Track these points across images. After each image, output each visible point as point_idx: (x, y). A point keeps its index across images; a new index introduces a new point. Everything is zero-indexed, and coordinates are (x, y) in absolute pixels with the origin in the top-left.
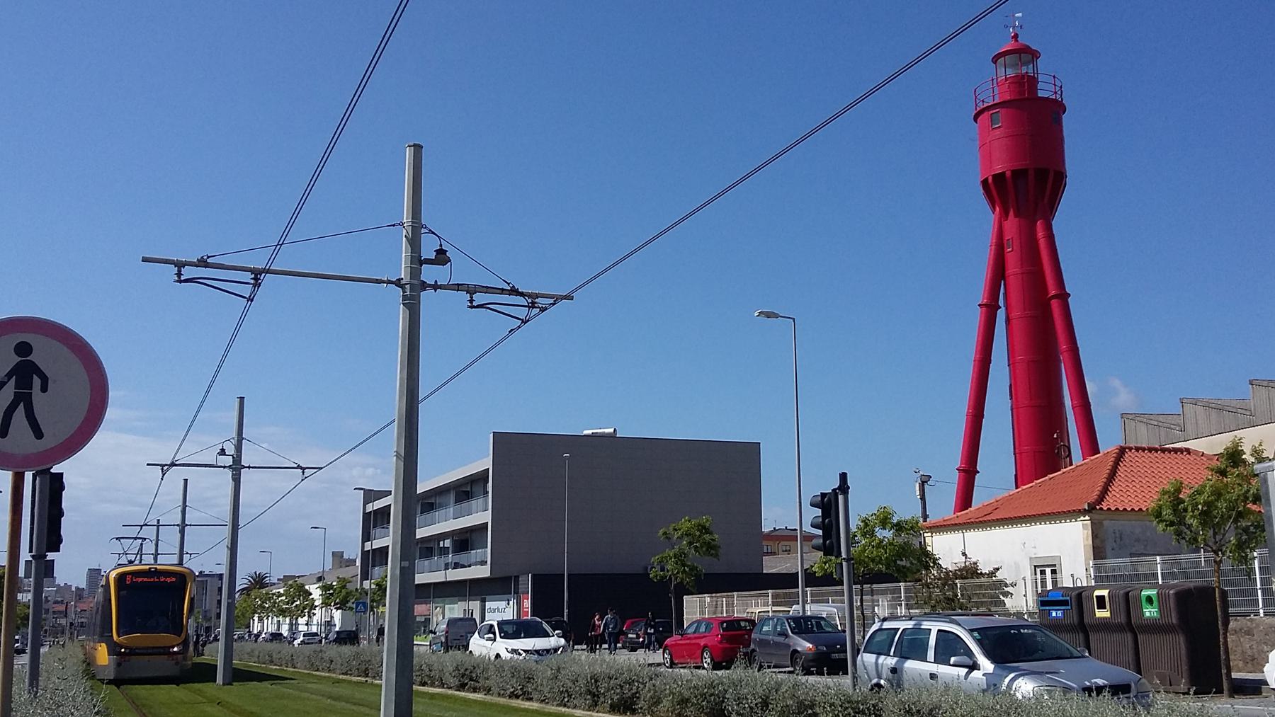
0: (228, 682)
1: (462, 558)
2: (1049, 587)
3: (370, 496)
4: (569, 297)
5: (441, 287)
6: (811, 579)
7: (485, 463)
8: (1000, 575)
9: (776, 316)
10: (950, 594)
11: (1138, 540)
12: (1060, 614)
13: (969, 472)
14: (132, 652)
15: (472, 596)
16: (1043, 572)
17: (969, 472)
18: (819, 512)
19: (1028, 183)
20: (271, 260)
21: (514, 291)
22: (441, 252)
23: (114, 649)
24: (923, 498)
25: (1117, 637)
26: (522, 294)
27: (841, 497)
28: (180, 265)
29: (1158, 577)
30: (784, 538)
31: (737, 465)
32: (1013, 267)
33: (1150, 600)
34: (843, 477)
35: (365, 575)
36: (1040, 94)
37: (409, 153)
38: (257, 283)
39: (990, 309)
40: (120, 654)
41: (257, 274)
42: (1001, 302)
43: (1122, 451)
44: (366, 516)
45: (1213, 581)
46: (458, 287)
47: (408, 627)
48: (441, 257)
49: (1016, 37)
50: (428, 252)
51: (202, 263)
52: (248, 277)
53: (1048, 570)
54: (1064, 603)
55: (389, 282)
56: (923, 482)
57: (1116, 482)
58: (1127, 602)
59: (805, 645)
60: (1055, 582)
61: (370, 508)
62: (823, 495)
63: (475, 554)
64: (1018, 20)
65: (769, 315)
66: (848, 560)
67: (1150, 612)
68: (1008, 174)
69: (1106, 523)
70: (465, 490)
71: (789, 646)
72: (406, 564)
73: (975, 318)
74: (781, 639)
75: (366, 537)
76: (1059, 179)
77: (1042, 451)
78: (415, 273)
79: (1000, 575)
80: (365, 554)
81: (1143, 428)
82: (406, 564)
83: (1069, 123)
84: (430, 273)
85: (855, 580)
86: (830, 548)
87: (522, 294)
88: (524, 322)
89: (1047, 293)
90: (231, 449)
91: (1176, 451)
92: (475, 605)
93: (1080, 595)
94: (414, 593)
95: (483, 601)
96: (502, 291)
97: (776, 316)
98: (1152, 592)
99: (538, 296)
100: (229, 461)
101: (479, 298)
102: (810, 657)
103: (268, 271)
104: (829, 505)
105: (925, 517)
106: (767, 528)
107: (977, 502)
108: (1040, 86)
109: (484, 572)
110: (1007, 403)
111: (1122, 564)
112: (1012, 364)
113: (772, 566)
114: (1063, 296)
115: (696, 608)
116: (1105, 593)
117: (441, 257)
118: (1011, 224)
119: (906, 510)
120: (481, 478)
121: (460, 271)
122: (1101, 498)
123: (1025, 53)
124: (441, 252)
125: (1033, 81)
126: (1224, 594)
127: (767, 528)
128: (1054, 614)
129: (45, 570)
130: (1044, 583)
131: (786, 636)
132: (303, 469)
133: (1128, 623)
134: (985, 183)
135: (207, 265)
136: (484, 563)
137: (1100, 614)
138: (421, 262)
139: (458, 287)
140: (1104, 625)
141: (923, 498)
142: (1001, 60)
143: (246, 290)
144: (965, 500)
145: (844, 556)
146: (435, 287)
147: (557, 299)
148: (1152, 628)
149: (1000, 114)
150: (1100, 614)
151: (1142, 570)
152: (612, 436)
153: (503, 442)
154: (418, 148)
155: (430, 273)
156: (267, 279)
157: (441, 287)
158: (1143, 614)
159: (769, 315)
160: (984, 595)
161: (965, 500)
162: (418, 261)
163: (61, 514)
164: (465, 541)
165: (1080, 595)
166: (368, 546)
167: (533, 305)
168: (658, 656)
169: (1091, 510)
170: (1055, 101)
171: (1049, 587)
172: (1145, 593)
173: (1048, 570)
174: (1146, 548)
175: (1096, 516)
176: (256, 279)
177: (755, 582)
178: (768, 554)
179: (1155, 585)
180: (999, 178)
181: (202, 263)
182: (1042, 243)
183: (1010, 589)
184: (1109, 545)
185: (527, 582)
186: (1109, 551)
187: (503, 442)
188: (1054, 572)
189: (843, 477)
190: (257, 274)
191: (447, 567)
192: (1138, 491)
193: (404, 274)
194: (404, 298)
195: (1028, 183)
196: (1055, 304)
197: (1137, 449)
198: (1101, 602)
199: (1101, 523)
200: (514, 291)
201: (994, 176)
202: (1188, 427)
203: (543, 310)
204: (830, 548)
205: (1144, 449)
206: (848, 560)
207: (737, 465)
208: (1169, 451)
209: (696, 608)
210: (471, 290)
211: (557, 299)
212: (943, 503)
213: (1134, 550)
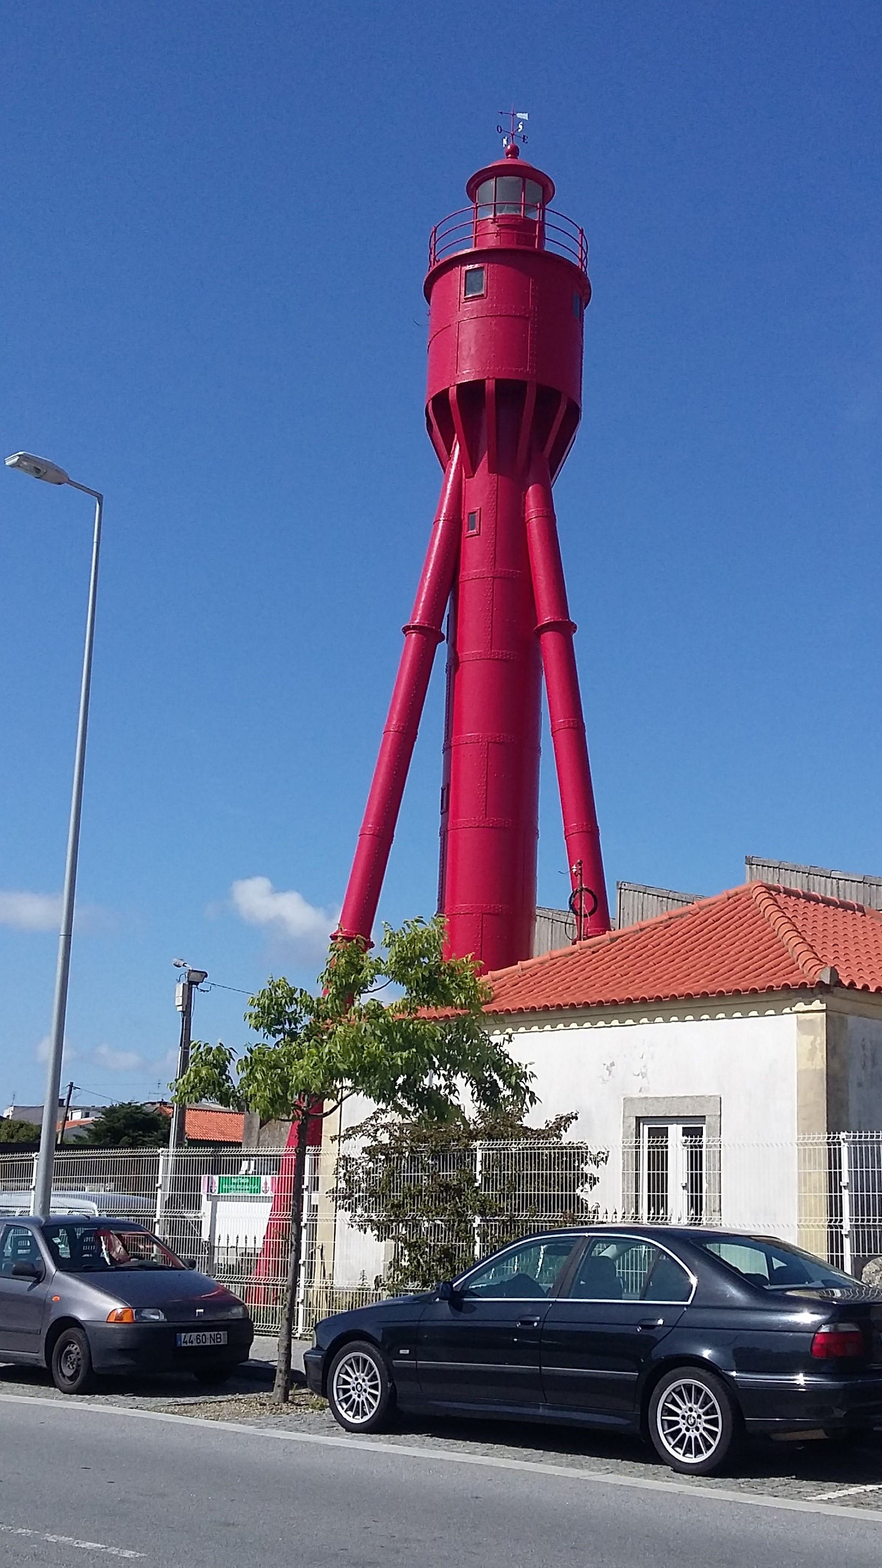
8: (569, 1137)
9: (60, 478)
10: (451, 1175)
16: (659, 1133)
19: (516, 419)
24: (187, 1013)
39: (428, 635)
49: (514, 152)
53: (675, 1131)
59: (96, 1305)
65: (39, 470)
68: (490, 385)
69: (851, 1020)
71: (43, 1305)
72: (689, 1418)
73: (397, 653)
74: (22, 1285)
76: (574, 414)
79: (569, 1137)
82: (689, 1418)
83: (598, 325)
97: (60, 478)
102: (118, 1341)
110: (435, 820)
114: (565, 628)
118: (481, 487)
123: (536, 183)
131: (38, 1275)
134: (440, 401)
141: (187, 1013)
149: (486, 275)
159: (39, 470)
160: (547, 1181)
173: (675, 1131)
175: (837, 1003)
180: (471, 391)
183: (590, 1169)
188: (693, 1133)
195: (516, 419)
196: (549, 641)
201: (460, 387)
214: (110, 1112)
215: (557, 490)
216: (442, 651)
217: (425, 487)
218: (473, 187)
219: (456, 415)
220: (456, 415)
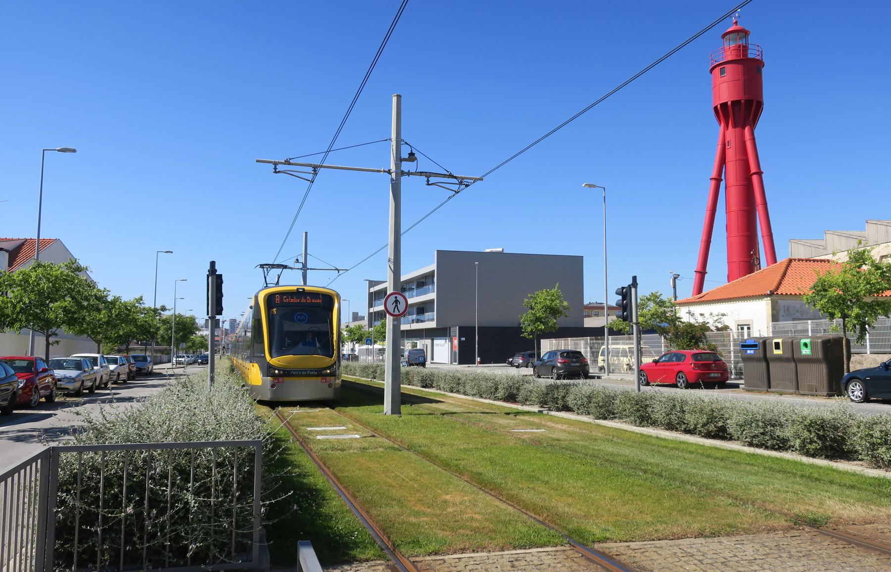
0: (396, 410)
1: (421, 317)
2: (746, 337)
3: (372, 284)
4: (481, 179)
5: (412, 174)
6: (612, 332)
7: (433, 267)
9: (594, 186)
11: (797, 311)
12: (752, 352)
13: (702, 273)
14: (286, 373)
15: (427, 337)
16: (742, 329)
17: (702, 273)
18: (620, 297)
19: (742, 112)
20: (324, 160)
21: (451, 176)
22: (412, 154)
23: (268, 370)
24: (675, 287)
25: (785, 365)
26: (456, 178)
27: (633, 290)
28: (275, 164)
29: (809, 334)
30: (596, 309)
31: (569, 270)
32: (731, 154)
33: (806, 345)
34: (634, 278)
35: (370, 325)
36: (750, 56)
37: (394, 99)
38: (315, 173)
39: (718, 180)
40: (274, 376)
41: (315, 168)
42: (723, 177)
43: (790, 261)
44: (370, 294)
45: (841, 334)
46: (421, 173)
47: (397, 353)
48: (412, 157)
50: (405, 155)
51: (287, 162)
52: (310, 169)
53: (745, 328)
54: (755, 346)
55: (384, 171)
56: (675, 278)
57: (786, 278)
58: (793, 346)
60: (749, 335)
61: (372, 290)
62: (623, 288)
63: (427, 315)
64: (742, 19)
65: (590, 186)
66: (637, 323)
67: (806, 351)
68: (729, 103)
70: (422, 282)
75: (371, 305)
76: (759, 105)
77: (746, 260)
78: (398, 166)
80: (370, 314)
81: (802, 247)
83: (766, 74)
84: (406, 166)
85: (639, 332)
86: (626, 319)
87: (456, 178)
88: (457, 192)
89: (750, 171)
90: (302, 260)
91: (821, 261)
92: (428, 342)
93: (764, 343)
94: (400, 336)
95: (433, 340)
96: (444, 176)
97: (594, 186)
98: (808, 341)
99: (463, 178)
100: (300, 266)
101: (432, 180)
103: (321, 167)
104: (625, 293)
105: (676, 297)
106: (586, 302)
107: (705, 290)
108: (749, 51)
109: (433, 325)
111: (787, 325)
112: (728, 212)
113: (589, 323)
114: (759, 173)
115: (547, 346)
116: (780, 341)
117: (412, 157)
119: (667, 295)
120: (430, 275)
121: (423, 165)
122: (777, 288)
123: (743, 33)
124: (412, 154)
125: (745, 49)
126: (848, 341)
127: (586, 302)
128: (749, 352)
129: (215, 324)
130: (743, 335)
132: (339, 270)
133: (793, 358)
134: (716, 108)
135: (289, 164)
136: (433, 320)
137: (776, 352)
138: (401, 160)
139: (421, 173)
140: (779, 359)
141: (675, 287)
142: (727, 37)
143: (310, 177)
144: (700, 289)
145: (634, 321)
146: (409, 174)
147: (475, 180)
148: (807, 360)
150: (776, 352)
151: (799, 328)
152: (501, 254)
153: (442, 256)
154: (399, 97)
155: (406, 166)
156: (321, 171)
157: (412, 174)
158: (801, 352)
159: (590, 186)
161: (700, 289)
162: (399, 160)
163: (222, 296)
164: (422, 309)
165: (764, 343)
166: (372, 310)
167: (461, 183)
168: (530, 371)
169: (771, 294)
170: (758, 60)
171: (746, 337)
172: (803, 341)
173: (745, 328)
174: (799, 315)
175: (774, 297)
176: (315, 171)
177: (580, 332)
178: (586, 316)
179: (807, 337)
180: (724, 105)
181: (287, 162)
182: (749, 144)
184: (781, 313)
185: (456, 331)
186: (781, 317)
187: (442, 256)
188: (749, 328)
189: (634, 278)
190: (315, 168)
191: (413, 321)
192: (800, 284)
193: (393, 168)
194: (392, 180)
196: (755, 178)
197: (799, 260)
198: (777, 346)
199: (777, 302)
200: (451, 176)
201: (721, 105)
202: (828, 246)
203: (467, 186)
204: (626, 319)
205: (802, 260)
206: (637, 323)
207: (569, 270)
208: (817, 261)
209: (547, 346)
210: (428, 175)
211: (475, 180)
212: (686, 290)
213: (795, 317)
214: (333, 408)
215: (755, 131)
216: (723, 184)
217: (714, 133)
218: (711, 71)
219: (723, 112)
220: (723, 112)
